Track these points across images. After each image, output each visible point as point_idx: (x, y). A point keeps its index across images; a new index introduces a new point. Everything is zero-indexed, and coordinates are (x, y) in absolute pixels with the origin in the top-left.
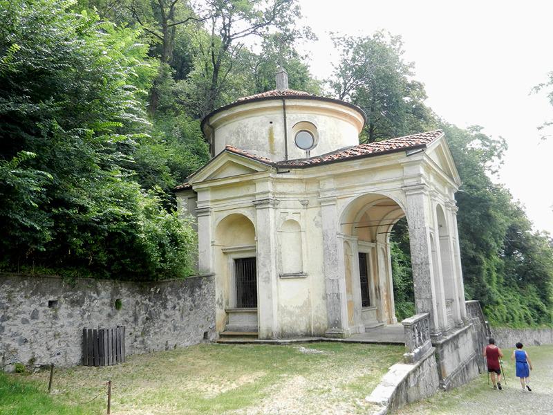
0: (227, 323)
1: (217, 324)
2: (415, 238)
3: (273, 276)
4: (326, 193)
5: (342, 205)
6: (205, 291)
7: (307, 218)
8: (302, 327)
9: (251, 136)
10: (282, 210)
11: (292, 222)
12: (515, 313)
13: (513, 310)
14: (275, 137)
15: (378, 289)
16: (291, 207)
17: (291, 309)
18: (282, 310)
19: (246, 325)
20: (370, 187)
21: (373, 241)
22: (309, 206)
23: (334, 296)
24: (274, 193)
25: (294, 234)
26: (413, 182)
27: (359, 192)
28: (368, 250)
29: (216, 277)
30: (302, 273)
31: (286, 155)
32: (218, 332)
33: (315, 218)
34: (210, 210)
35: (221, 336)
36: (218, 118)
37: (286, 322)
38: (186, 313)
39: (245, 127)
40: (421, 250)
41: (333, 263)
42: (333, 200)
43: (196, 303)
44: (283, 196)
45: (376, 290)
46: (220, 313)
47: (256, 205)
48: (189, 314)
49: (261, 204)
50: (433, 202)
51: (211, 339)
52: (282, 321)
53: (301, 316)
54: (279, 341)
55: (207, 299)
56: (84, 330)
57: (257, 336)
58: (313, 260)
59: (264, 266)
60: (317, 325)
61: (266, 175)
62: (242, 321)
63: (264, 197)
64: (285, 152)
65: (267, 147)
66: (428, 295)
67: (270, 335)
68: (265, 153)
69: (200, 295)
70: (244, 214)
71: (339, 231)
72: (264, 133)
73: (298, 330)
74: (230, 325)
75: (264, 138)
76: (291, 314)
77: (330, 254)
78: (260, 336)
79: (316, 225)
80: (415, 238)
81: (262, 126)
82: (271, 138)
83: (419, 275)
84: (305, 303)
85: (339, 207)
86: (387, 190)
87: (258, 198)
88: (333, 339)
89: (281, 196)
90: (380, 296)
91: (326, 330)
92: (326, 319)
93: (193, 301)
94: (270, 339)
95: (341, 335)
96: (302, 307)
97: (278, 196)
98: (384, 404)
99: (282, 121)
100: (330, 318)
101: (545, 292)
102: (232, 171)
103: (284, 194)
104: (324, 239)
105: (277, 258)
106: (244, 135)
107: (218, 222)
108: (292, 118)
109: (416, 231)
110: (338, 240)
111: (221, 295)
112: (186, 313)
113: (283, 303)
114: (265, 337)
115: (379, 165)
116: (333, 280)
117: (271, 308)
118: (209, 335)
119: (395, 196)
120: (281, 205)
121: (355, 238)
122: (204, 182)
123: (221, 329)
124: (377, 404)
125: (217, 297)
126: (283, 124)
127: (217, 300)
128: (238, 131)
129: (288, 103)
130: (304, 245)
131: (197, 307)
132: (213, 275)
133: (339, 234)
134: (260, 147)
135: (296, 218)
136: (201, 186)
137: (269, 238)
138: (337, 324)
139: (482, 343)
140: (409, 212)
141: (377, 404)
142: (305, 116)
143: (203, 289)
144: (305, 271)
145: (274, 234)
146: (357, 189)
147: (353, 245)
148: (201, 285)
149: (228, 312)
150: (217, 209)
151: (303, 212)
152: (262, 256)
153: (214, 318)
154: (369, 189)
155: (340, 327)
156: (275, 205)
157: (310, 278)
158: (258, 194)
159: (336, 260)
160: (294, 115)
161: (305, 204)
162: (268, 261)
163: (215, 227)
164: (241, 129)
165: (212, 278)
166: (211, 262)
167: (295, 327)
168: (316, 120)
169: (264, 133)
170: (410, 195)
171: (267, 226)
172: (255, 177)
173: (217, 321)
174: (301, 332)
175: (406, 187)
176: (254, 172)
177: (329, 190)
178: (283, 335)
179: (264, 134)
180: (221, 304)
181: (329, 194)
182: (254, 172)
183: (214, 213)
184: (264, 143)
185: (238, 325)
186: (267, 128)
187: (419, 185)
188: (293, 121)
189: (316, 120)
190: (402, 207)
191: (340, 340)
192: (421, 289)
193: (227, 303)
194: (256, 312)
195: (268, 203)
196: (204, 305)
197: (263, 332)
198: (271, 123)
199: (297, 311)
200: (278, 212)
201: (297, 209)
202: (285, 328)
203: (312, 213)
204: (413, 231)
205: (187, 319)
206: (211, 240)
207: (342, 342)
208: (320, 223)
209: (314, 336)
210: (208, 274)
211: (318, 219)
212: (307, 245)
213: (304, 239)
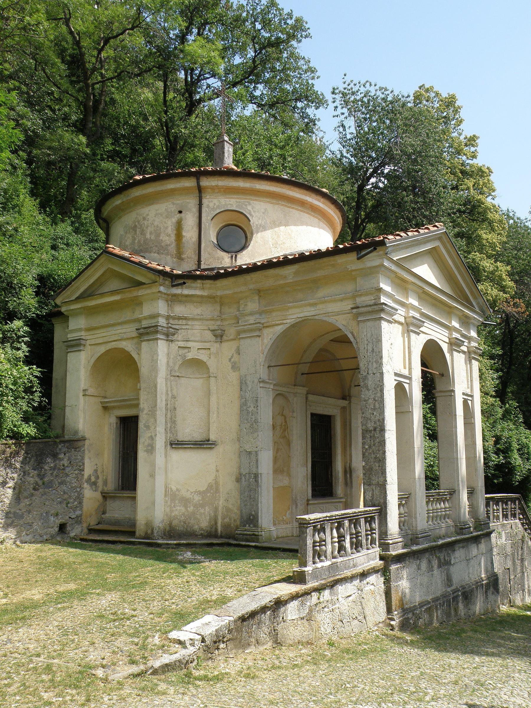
0: (104, 513)
1: (84, 514)
2: (368, 390)
3: (160, 442)
4: (247, 318)
5: (269, 336)
6: (66, 462)
7: (218, 357)
8: (203, 523)
9: (151, 233)
10: (182, 344)
11: (197, 364)
14: (184, 234)
15: (349, 471)
16: (196, 338)
17: (188, 495)
18: (172, 495)
19: (127, 516)
20: (308, 308)
21: (344, 398)
22: (225, 338)
23: (250, 478)
24: (168, 318)
25: (201, 381)
26: (368, 300)
27: (295, 314)
28: (329, 407)
29: (87, 442)
30: (208, 440)
31: (199, 261)
32: (85, 525)
33: (232, 357)
34: (83, 342)
35: (91, 531)
36: (111, 207)
37: (177, 513)
38: (25, 494)
39: (144, 219)
41: (251, 427)
42: (259, 329)
43: (46, 479)
44: (184, 322)
45: (345, 472)
46: (90, 496)
47: (141, 335)
48: (32, 495)
49: (147, 334)
50: (413, 336)
51: (72, 534)
52: (172, 511)
53: (203, 506)
54: (160, 542)
55: (67, 475)
57: (132, 534)
58: (224, 422)
59: (148, 427)
60: (227, 520)
61: (154, 290)
62: (117, 511)
63: (151, 322)
64: (197, 258)
65: (172, 249)
66: (381, 479)
67: (149, 532)
69: (54, 468)
70: (126, 349)
71: (265, 377)
72: (170, 228)
73: (196, 527)
74: (107, 515)
75: (169, 236)
76: (185, 502)
77: (248, 412)
78: (137, 534)
79: (233, 367)
80: (368, 390)
81: (167, 217)
82: (179, 236)
83: (370, 447)
84: (210, 486)
85: (265, 341)
86: (327, 314)
87: (145, 324)
88: (244, 543)
89: (180, 322)
90: (351, 482)
91: (237, 528)
92: (238, 512)
93: (41, 477)
94: (148, 538)
95: (255, 537)
96: (204, 492)
97: (176, 322)
98: (193, 645)
99: (195, 210)
100: (244, 511)
102: (114, 284)
103: (186, 318)
105: (169, 415)
106: (143, 233)
107: (93, 360)
108: (211, 205)
109: (370, 377)
110: (261, 391)
111: (96, 471)
112: (25, 494)
113: (175, 482)
114: (143, 534)
115: (320, 273)
116: (250, 453)
117: (153, 492)
118: (68, 528)
119: (344, 323)
120: (179, 336)
121: (302, 391)
122: (81, 297)
123: (93, 522)
125: (88, 471)
126: (197, 214)
127: (86, 477)
128: (136, 226)
129: (205, 182)
130: (214, 399)
131: (48, 485)
132: (84, 439)
133: (263, 382)
134: (162, 249)
135: (203, 356)
136: (73, 307)
137: (156, 386)
138: (252, 519)
139: (522, 560)
140: (361, 348)
142: (232, 203)
143: (61, 460)
144: (212, 437)
145: (166, 379)
146: (291, 311)
147: (297, 402)
148: (58, 454)
149: (105, 496)
150: (93, 342)
151: (215, 347)
152: (145, 412)
153: (80, 503)
154: (308, 312)
155: (256, 525)
156: (169, 335)
157: (219, 449)
158: (145, 318)
159: (256, 421)
160: (215, 201)
161: (219, 336)
163: (90, 368)
164: (139, 222)
165: (80, 444)
166: (81, 421)
167: (192, 522)
168: (249, 208)
169: (170, 228)
170: (364, 321)
171: (154, 368)
172: (141, 292)
173: (85, 508)
174: (202, 529)
175: (358, 307)
176: (140, 284)
177: (251, 314)
178: (170, 532)
179: (169, 230)
180: (95, 484)
181: (252, 319)
182: (140, 284)
183: (89, 347)
184: (169, 243)
185: (117, 516)
186: (174, 220)
187: (375, 304)
188: (213, 209)
189: (249, 208)
190: (352, 339)
191: (253, 544)
193: (105, 483)
194: (134, 498)
195: (157, 332)
196: (61, 483)
197: (141, 528)
198: (180, 212)
199: (197, 498)
200: (174, 347)
201: (205, 342)
202: (175, 523)
203: (228, 349)
204: (365, 378)
205: (27, 502)
206: (83, 386)
207: (256, 547)
209: (221, 537)
210: (76, 438)
211: (236, 358)
213: (213, 388)
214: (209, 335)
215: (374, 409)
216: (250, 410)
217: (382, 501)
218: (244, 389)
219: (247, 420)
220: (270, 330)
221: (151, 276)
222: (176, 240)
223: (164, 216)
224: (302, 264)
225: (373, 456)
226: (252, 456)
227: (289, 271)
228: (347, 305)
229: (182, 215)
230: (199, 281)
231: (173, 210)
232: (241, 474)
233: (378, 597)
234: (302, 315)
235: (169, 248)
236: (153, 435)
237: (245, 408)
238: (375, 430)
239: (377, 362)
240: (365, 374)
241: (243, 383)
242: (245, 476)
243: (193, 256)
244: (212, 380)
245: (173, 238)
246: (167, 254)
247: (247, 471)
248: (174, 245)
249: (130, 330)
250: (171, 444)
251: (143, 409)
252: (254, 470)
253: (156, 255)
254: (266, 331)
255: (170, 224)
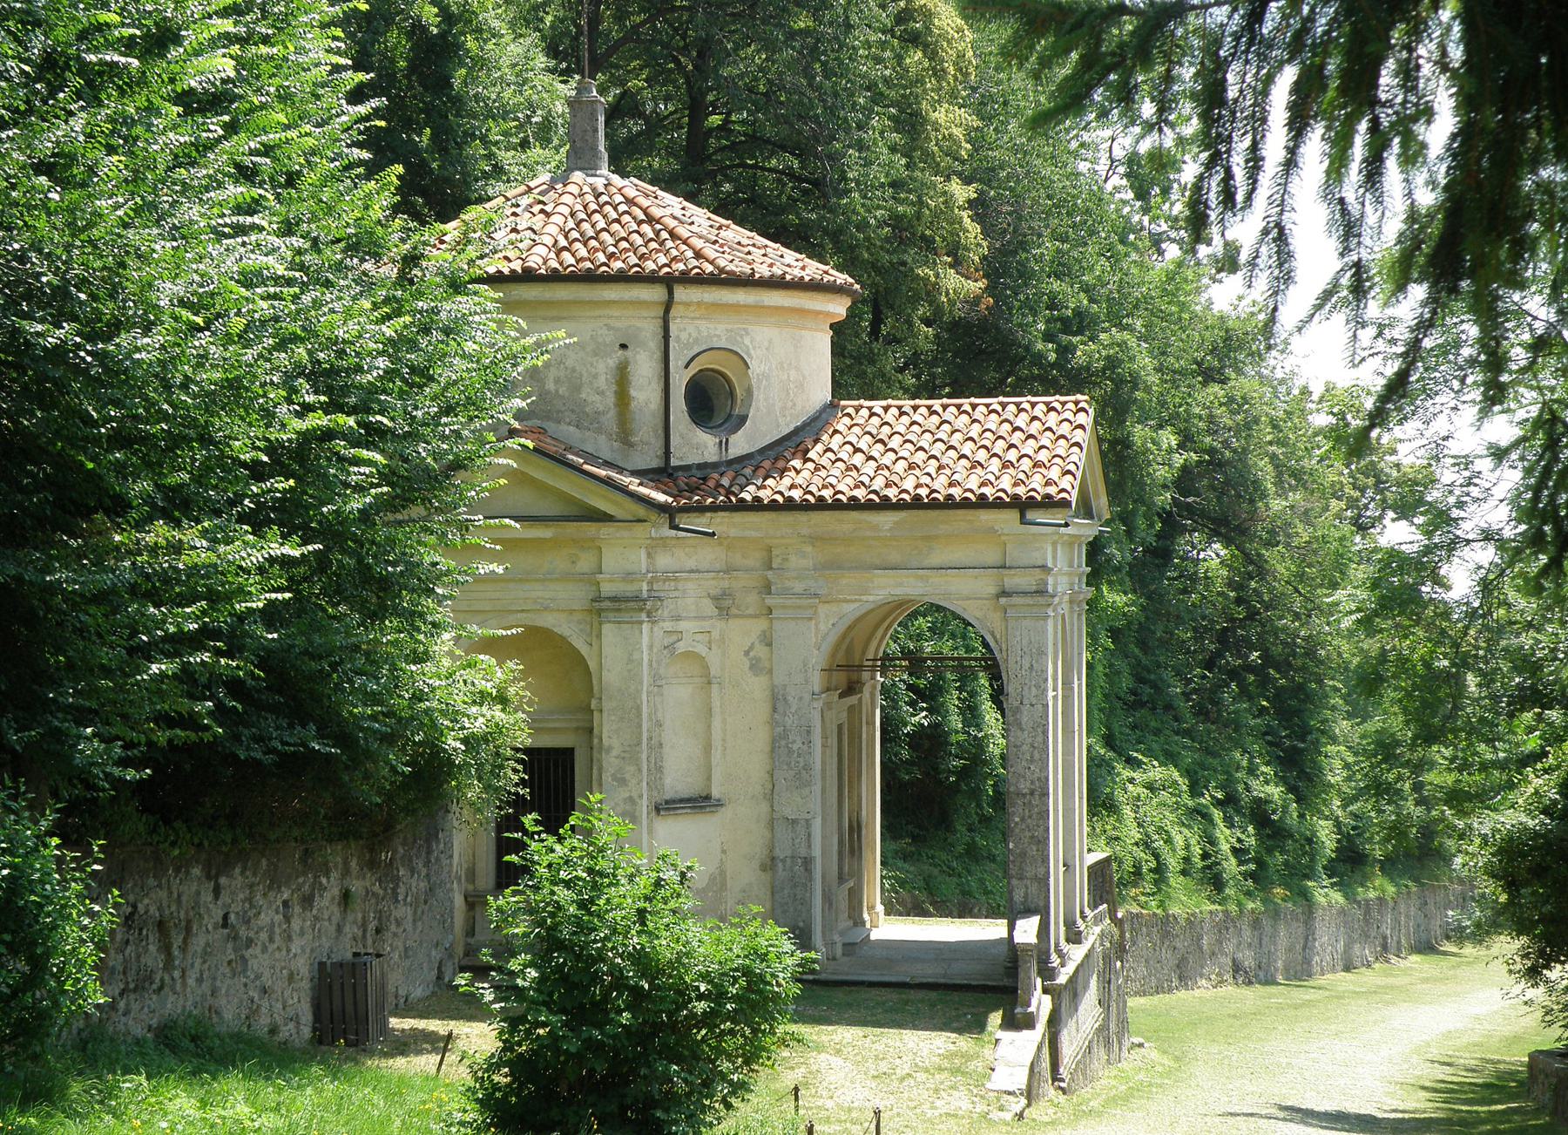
2: (1022, 730)
9: (557, 381)
10: (668, 625)
12: (1169, 841)
13: (1160, 830)
14: (633, 393)
33: (751, 648)
40: (1032, 761)
45: (851, 827)
56: (322, 965)
58: (740, 761)
64: (661, 442)
65: (610, 420)
66: (1042, 870)
68: (602, 439)
72: (602, 378)
75: (602, 393)
79: (752, 667)
80: (1022, 730)
83: (1023, 819)
84: (712, 879)
90: (860, 848)
99: (654, 344)
101: (1303, 733)
104: (775, 710)
109: (1026, 709)
116: (794, 822)
124: (1010, 1093)
129: (681, 293)
130: (717, 723)
137: (639, 709)
141: (1010, 1093)
144: (715, 793)
151: (717, 627)
152: (614, 753)
157: (725, 814)
162: (632, 768)
176: (605, 518)
179: (602, 382)
186: (612, 362)
188: (688, 346)
192: (1023, 854)
198: (624, 346)
208: (767, 665)
211: (761, 651)
212: (724, 721)
213: (716, 704)
214: (709, 607)
215: (1032, 761)
216: (795, 747)
217: (1041, 904)
218: (780, 709)
219: (788, 764)
220: (834, 608)
221: (641, 511)
222: (616, 405)
223: (589, 349)
224: (915, 512)
225: (1028, 834)
226: (798, 828)
227: (887, 519)
228: (986, 585)
229: (628, 353)
230: (708, 514)
231: (608, 340)
232: (773, 859)
233: (880, 1047)
234: (898, 591)
235: (603, 419)
236: (635, 795)
237: (783, 743)
238: (1032, 793)
239: (1038, 687)
240: (1016, 704)
241: (777, 700)
242: (783, 861)
243: (653, 441)
244: (715, 688)
245: (611, 399)
246: (599, 431)
247: (789, 853)
248: (612, 413)
249: (575, 595)
250: (658, 810)
251: (610, 748)
252: (803, 852)
253: (571, 428)
254: (823, 609)
255: (604, 368)
